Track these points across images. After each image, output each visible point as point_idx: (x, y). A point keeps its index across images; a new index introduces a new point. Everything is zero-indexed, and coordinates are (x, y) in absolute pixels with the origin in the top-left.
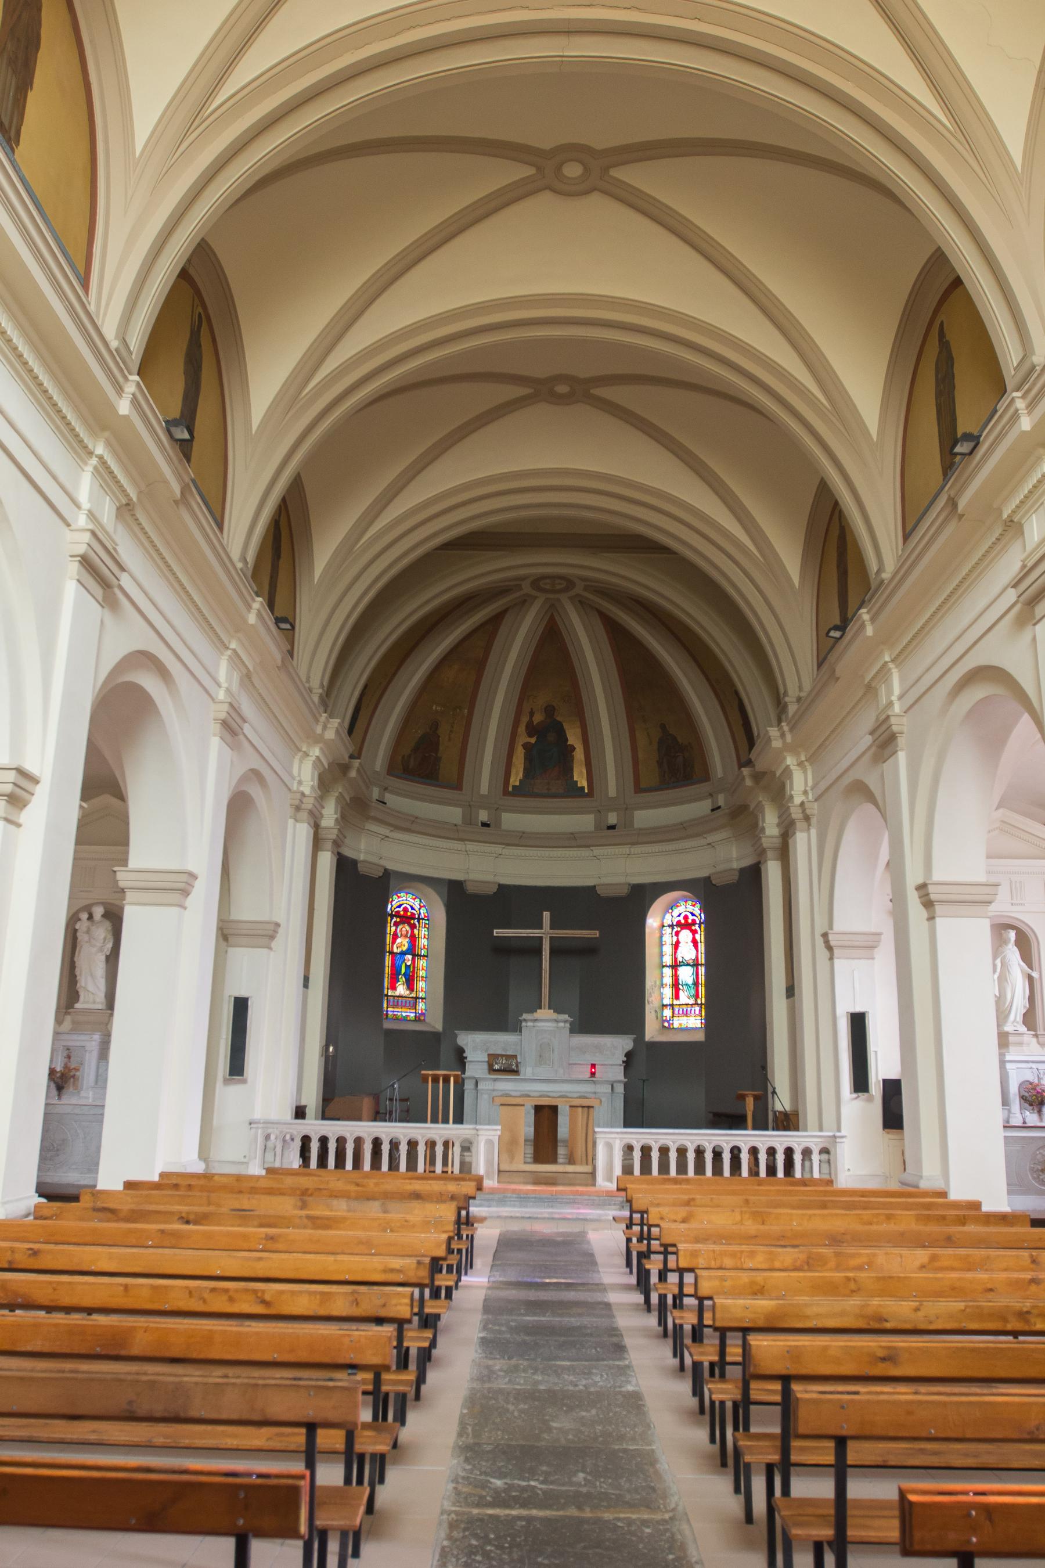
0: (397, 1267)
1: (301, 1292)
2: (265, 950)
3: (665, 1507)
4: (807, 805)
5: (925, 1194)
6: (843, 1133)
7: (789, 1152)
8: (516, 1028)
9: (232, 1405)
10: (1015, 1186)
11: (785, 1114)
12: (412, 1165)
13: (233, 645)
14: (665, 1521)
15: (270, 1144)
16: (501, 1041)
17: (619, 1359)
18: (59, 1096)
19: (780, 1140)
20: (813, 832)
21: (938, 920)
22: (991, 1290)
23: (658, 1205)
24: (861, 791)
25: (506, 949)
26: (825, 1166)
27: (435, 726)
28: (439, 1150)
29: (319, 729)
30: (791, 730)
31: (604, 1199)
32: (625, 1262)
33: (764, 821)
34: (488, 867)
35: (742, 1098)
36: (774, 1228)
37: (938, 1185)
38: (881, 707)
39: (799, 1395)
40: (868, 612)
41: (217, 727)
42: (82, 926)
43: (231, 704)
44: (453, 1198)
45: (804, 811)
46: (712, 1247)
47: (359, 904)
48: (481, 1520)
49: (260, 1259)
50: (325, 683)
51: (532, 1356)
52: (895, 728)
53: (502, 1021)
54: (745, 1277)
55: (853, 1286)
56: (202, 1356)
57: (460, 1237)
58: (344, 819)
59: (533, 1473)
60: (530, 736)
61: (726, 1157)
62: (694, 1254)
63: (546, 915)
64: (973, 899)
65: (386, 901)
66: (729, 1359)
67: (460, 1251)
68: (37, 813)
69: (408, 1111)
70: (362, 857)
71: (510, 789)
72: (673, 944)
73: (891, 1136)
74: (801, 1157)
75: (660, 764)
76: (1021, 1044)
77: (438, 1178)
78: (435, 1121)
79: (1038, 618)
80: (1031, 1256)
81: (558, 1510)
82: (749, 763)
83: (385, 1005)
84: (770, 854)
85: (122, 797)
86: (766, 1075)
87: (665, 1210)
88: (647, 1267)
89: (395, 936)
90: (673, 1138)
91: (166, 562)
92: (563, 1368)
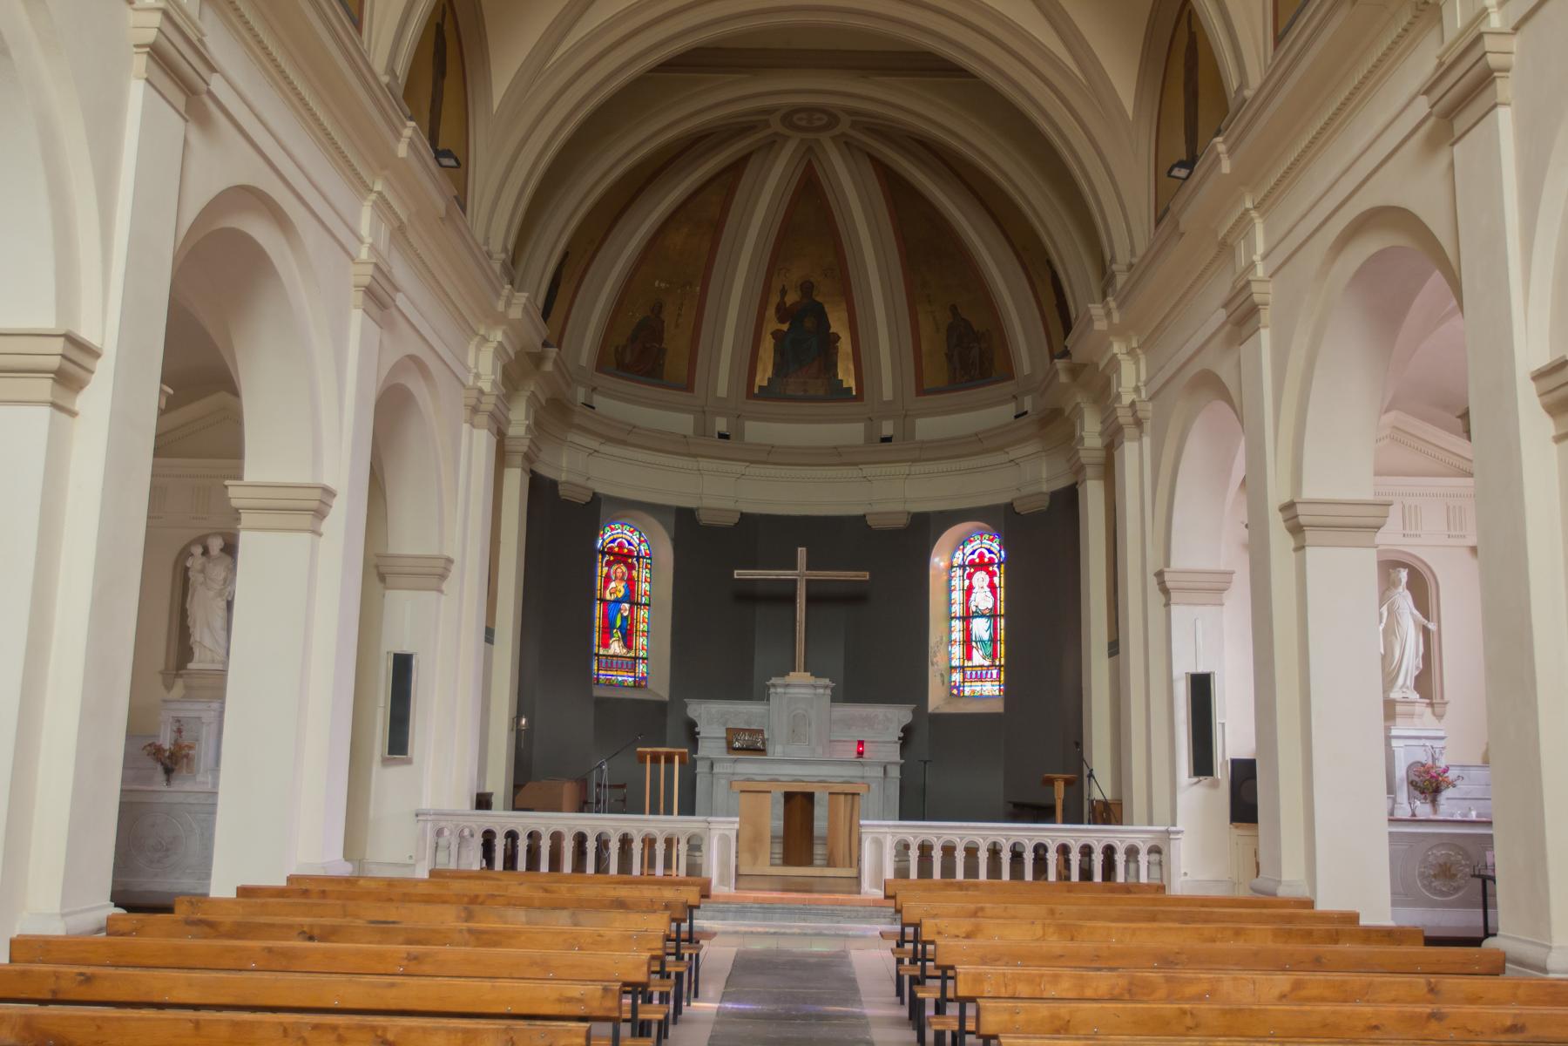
0: (576, 994)
1: (436, 1029)
2: (434, 593)
4: (1138, 406)
5: (1286, 903)
6: (1179, 827)
7: (1109, 851)
8: (763, 696)
10: (1402, 895)
12: (625, 865)
13: (378, 187)
15: (443, 842)
16: (743, 713)
18: (168, 781)
19: (1097, 836)
20: (1147, 441)
21: (1309, 551)
22: (1376, 1027)
23: (935, 916)
24: (1210, 385)
25: (750, 595)
26: (1155, 869)
27: (658, 308)
28: (660, 848)
29: (501, 306)
30: (1120, 306)
31: (869, 911)
33: (1082, 429)
34: (726, 490)
36: (1086, 945)
37: (1303, 892)
38: (1239, 271)
40: (1224, 142)
41: (359, 296)
42: (195, 563)
43: (376, 266)
44: (667, 907)
45: (1134, 413)
46: (1001, 969)
47: (558, 541)
49: (392, 985)
50: (510, 247)
52: (1257, 298)
53: (744, 686)
55: (1189, 1021)
57: (680, 957)
58: (538, 427)
60: (782, 321)
61: (1029, 857)
62: (978, 979)
63: (802, 552)
64: (1358, 523)
65: (594, 534)
67: (679, 976)
68: (97, 398)
69: (624, 801)
70: (563, 477)
71: (756, 390)
72: (965, 591)
75: (949, 357)
76: (1411, 715)
77: (660, 883)
79: (1457, 134)
80: (1429, 983)
82: (1066, 354)
84: (1089, 471)
85: (235, 393)
87: (943, 923)
88: (920, 995)
89: (608, 580)
90: (959, 833)
91: (278, 66)
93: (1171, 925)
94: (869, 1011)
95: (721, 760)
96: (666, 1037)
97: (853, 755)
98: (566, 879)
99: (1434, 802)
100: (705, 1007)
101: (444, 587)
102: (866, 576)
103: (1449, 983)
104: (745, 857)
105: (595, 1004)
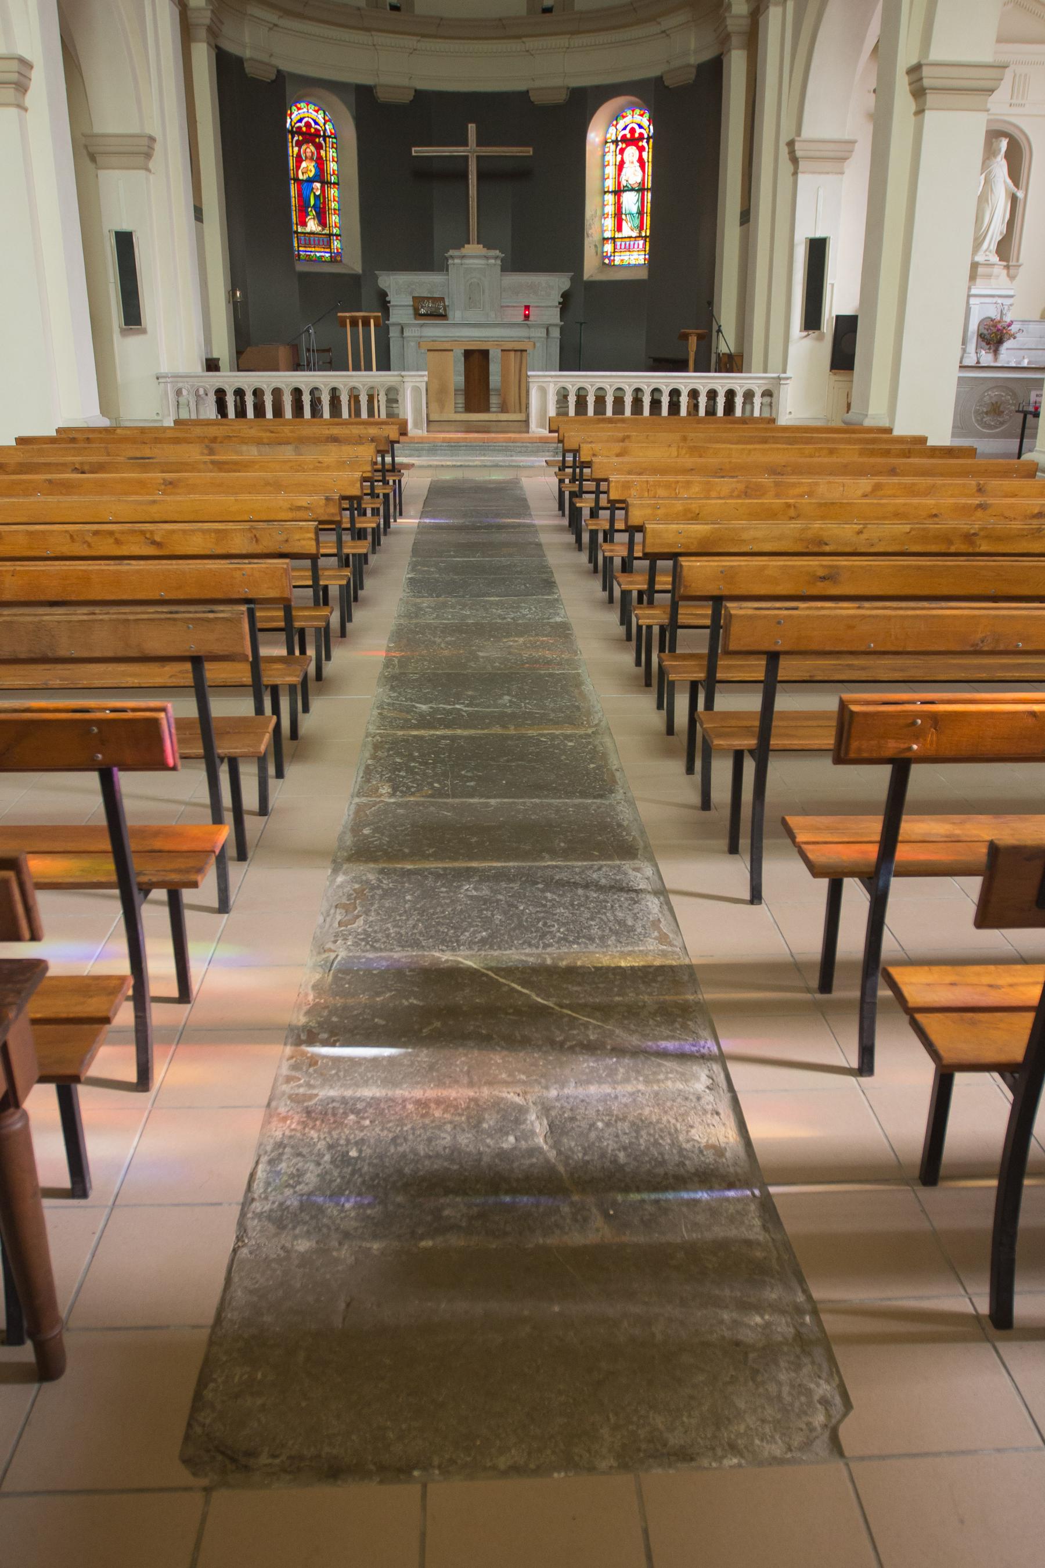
0: (305, 504)
1: (193, 531)
2: (143, 172)
3: (588, 723)
7: (730, 394)
8: (442, 267)
9: (103, 642)
10: (960, 427)
11: (730, 356)
14: (588, 736)
15: (182, 400)
16: (426, 282)
17: (548, 594)
19: (720, 382)
21: (927, 112)
22: (935, 516)
25: (429, 173)
26: (766, 409)
32: (557, 506)
35: (685, 337)
36: (712, 461)
37: (885, 423)
39: (733, 612)
47: (249, 115)
48: (407, 741)
51: (461, 593)
53: (427, 259)
54: (679, 506)
55: (792, 512)
56: (82, 598)
57: (386, 482)
59: (458, 698)
62: (626, 486)
63: (472, 127)
66: (657, 587)
67: (386, 496)
69: (330, 363)
70: (247, 54)
72: (617, 161)
73: (837, 378)
74: (742, 400)
76: (989, 276)
78: (356, 368)
80: (979, 485)
81: (482, 729)
83: (296, 245)
84: (735, 40)
86: (712, 310)
87: (597, 447)
88: (578, 505)
89: (299, 160)
92: (492, 603)
93: (779, 446)
94: (537, 522)
95: (409, 325)
96: (379, 544)
97: (520, 318)
98: (288, 423)
99: (996, 352)
100: (408, 522)
101: (151, 165)
102: (529, 151)
103: (994, 483)
104: (434, 406)
105: (320, 511)
